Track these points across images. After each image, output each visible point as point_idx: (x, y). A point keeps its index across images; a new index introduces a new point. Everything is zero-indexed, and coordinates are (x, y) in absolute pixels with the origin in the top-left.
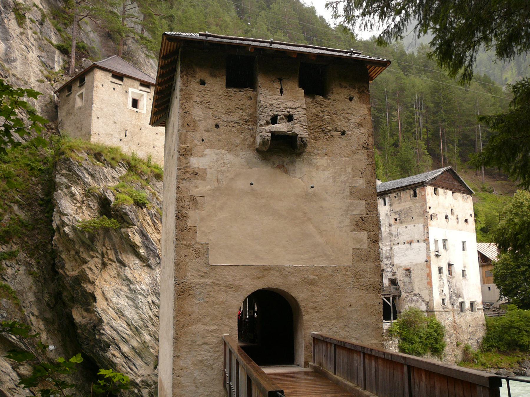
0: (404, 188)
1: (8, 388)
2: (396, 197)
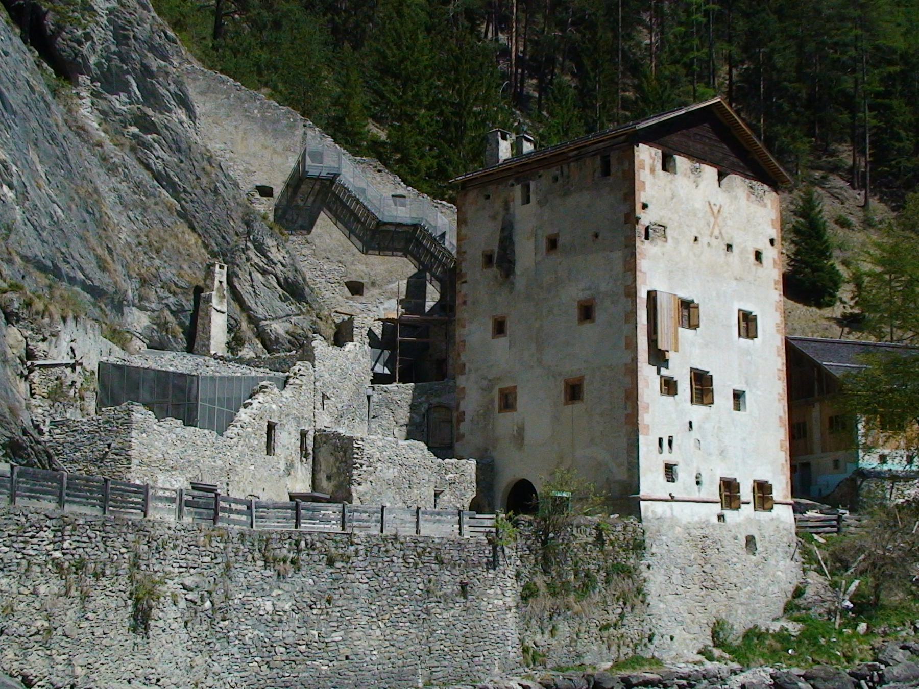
1: (394, 533)
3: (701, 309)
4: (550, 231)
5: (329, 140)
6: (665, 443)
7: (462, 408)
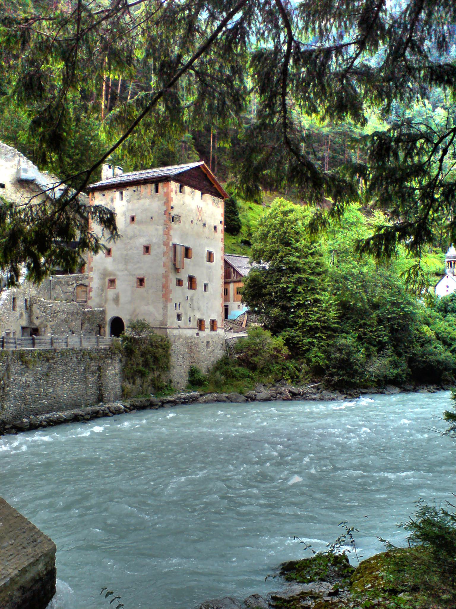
0: (145, 182)
2: (135, 191)
3: (193, 251)
4: (132, 214)
5: (30, 163)
6: (178, 305)
7: (91, 286)
